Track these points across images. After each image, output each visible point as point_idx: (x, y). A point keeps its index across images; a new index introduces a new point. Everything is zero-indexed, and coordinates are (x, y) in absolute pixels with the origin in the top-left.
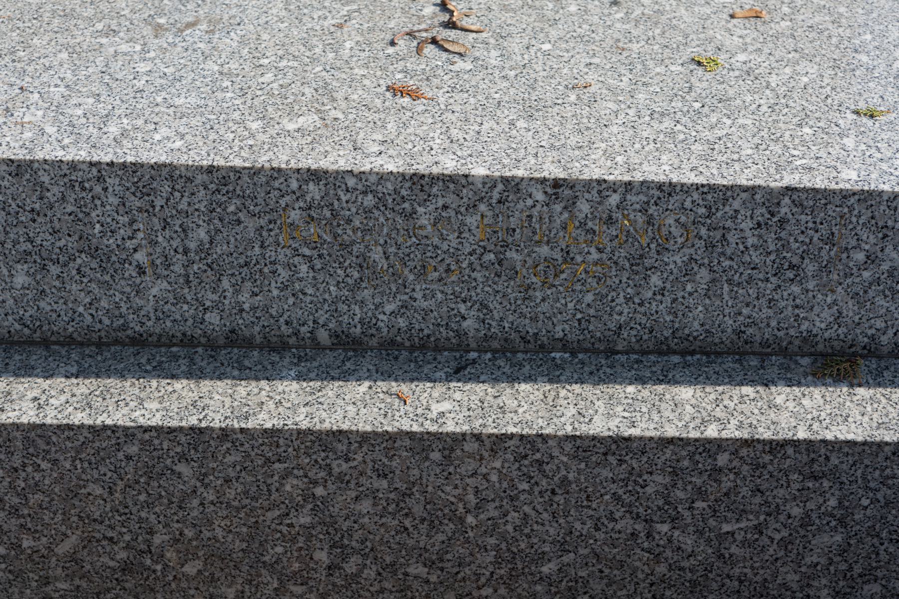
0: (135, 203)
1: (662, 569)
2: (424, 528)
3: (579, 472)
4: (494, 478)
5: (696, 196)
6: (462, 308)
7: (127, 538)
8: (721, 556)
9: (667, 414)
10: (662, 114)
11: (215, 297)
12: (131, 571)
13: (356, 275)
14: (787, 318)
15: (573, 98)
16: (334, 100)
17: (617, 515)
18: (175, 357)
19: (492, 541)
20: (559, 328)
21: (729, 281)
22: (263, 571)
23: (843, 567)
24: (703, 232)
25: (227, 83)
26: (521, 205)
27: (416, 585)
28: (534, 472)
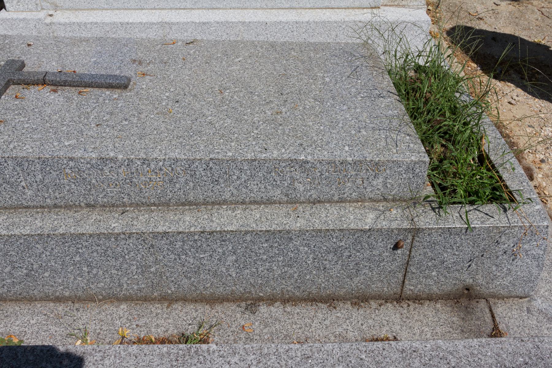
0: (18, 169)
1: (185, 268)
2: (114, 260)
3: (156, 242)
4: (131, 245)
5: (184, 162)
6: (123, 195)
7: (25, 266)
8: (202, 264)
9: (180, 224)
10: (180, 137)
11: (48, 195)
12: (29, 276)
13: (89, 187)
14: (217, 195)
15: (155, 132)
16: (83, 135)
17: (169, 254)
18: (38, 212)
19: (135, 262)
20: (152, 200)
21: (199, 185)
22: (69, 274)
23: (237, 265)
24: (189, 172)
25: (51, 130)
26: (134, 166)
27: (115, 276)
28: (142, 243)
